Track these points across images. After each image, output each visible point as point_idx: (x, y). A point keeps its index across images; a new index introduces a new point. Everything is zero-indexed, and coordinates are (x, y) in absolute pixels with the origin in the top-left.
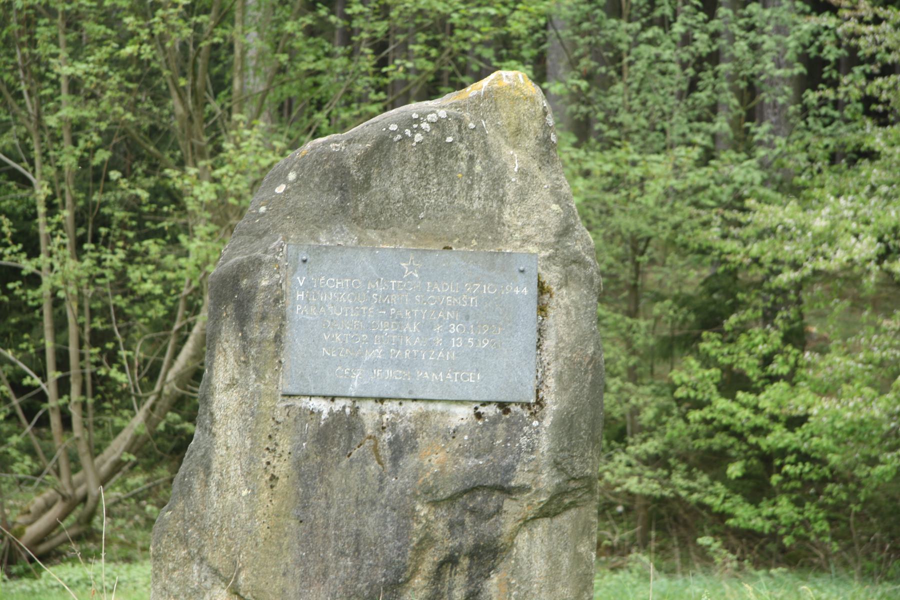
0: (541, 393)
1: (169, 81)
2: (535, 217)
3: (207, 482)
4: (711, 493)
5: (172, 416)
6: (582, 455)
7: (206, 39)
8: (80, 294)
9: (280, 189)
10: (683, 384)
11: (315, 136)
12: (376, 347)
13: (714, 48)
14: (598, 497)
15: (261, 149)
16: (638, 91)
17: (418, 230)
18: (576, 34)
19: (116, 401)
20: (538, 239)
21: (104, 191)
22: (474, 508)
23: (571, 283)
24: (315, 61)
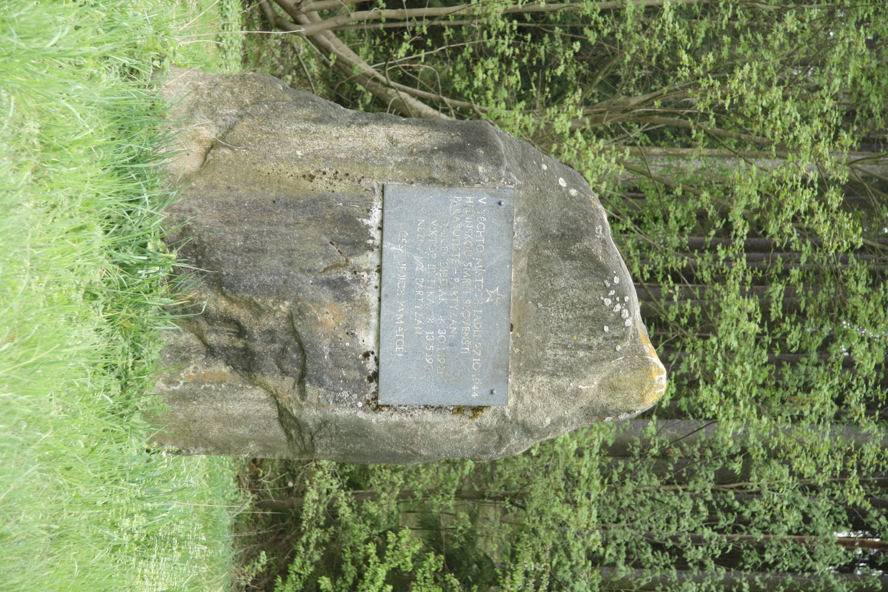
0: (386, 409)
1: (658, 92)
2: (539, 404)
3: (308, 120)
4: (304, 563)
5: (369, 97)
6: (333, 445)
7: (695, 124)
8: (474, 17)
9: (562, 182)
10: (399, 538)
11: (611, 218)
12: (425, 266)
13: (690, 565)
14: (297, 459)
15: (599, 171)
16: (652, 499)
17: (527, 302)
18: (702, 443)
19: (381, 49)
20: (520, 406)
21: (562, 37)
22: (286, 352)
23: (482, 434)
24: (676, 218)
